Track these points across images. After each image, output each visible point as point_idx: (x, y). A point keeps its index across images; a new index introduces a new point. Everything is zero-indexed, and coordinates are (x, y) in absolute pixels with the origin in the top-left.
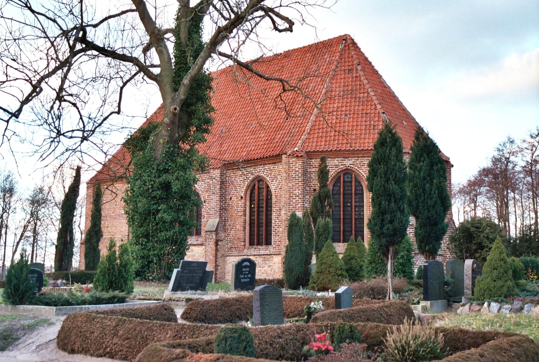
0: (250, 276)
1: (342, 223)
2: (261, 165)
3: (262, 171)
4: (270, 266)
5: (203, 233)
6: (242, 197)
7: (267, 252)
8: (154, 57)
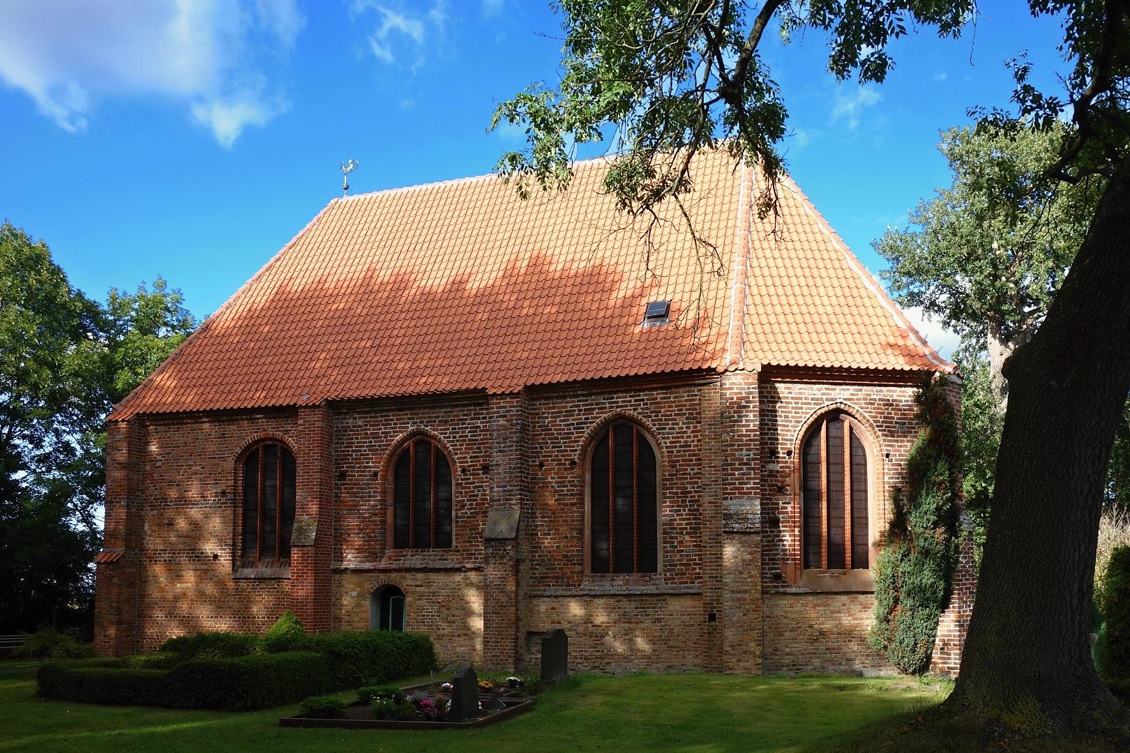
4: (659, 620)
7: (651, 589)
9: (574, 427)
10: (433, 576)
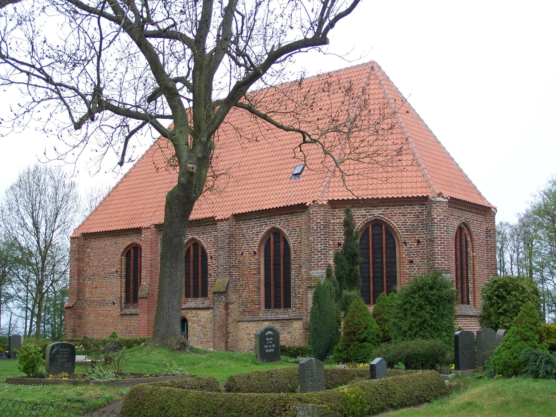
0: (274, 346)
1: (371, 282)
2: (277, 215)
3: (278, 223)
4: (290, 332)
5: (210, 295)
6: (255, 253)
7: (286, 317)
8: (162, 106)
9: (256, 233)
10: (199, 312)
